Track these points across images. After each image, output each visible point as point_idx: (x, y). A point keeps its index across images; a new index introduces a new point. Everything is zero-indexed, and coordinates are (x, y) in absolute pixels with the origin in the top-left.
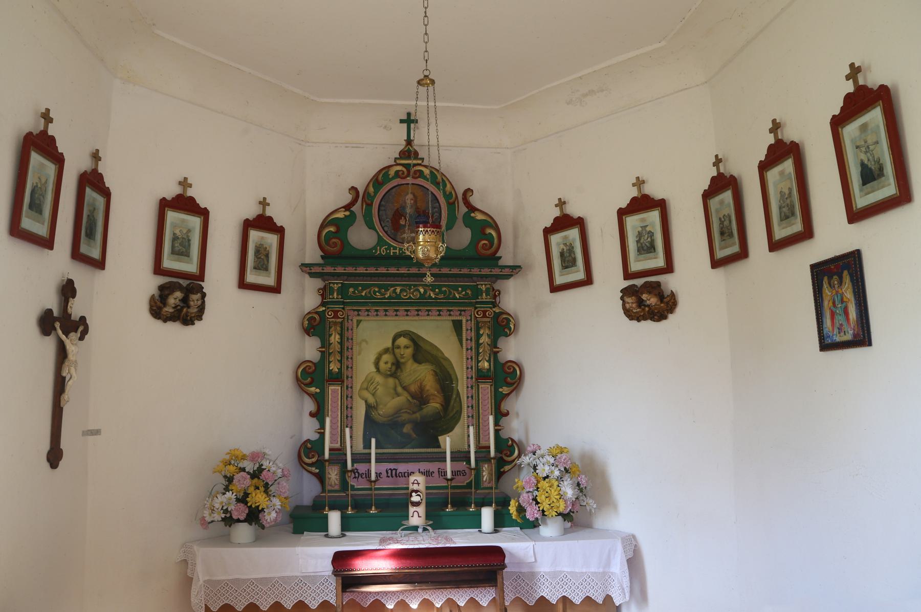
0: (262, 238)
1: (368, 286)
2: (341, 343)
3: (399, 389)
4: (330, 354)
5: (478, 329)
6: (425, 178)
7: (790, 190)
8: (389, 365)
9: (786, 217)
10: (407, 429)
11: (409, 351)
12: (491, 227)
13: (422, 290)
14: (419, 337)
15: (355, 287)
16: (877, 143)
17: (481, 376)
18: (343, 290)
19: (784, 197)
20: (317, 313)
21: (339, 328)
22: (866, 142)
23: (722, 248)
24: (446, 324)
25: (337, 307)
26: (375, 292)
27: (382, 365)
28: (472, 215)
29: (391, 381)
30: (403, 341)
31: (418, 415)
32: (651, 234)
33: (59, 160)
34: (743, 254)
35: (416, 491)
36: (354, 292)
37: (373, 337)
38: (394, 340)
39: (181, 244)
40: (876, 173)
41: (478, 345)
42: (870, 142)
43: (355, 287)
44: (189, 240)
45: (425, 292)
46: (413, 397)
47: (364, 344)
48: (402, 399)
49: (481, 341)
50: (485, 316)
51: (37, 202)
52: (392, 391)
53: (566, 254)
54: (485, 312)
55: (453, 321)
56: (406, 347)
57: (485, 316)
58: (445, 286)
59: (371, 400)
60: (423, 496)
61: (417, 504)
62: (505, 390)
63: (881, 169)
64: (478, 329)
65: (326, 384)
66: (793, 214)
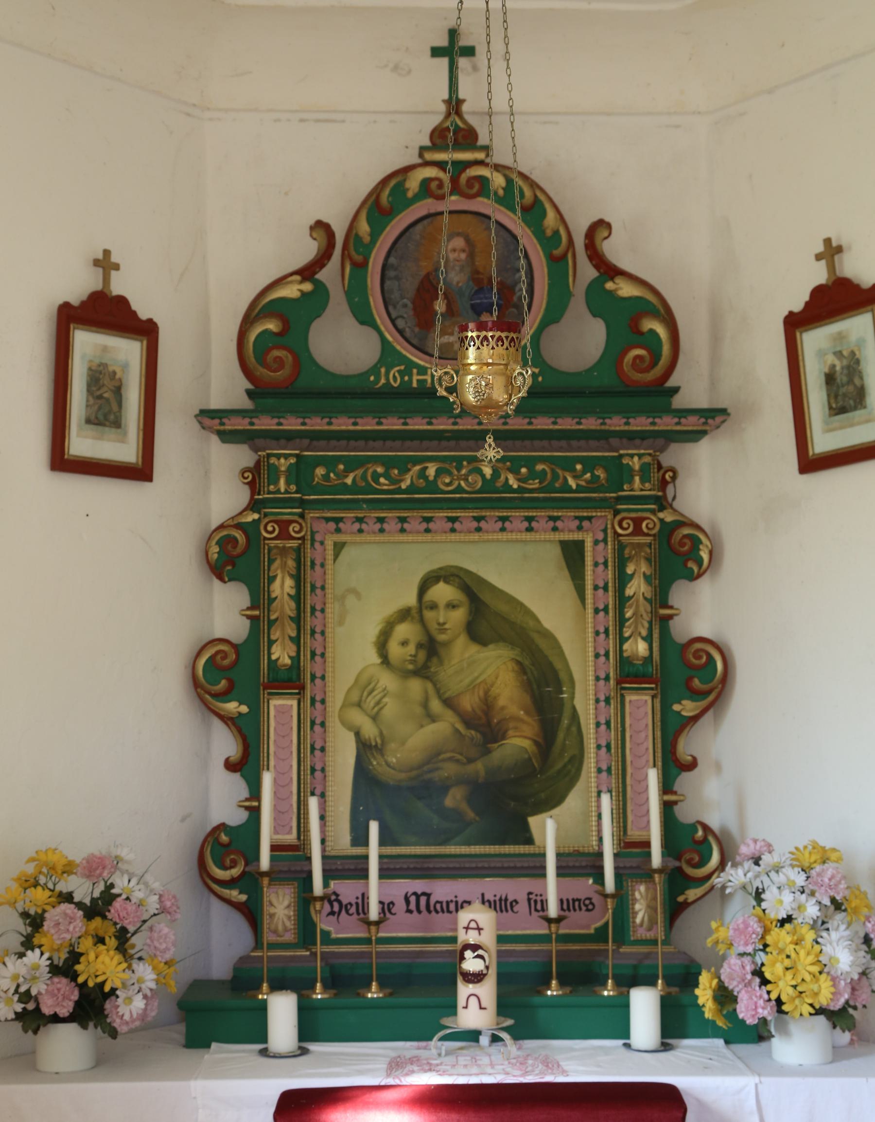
0: (105, 349)
1: (362, 463)
2: (298, 598)
3: (436, 705)
4: (271, 623)
5: (621, 563)
8: (411, 649)
10: (454, 799)
11: (459, 616)
15: (330, 463)
17: (630, 675)
18: (300, 472)
21: (291, 563)
24: (544, 550)
25: (287, 513)
26: (376, 477)
27: (395, 650)
29: (416, 686)
30: (442, 592)
31: (479, 767)
35: (475, 947)
36: (326, 477)
38: (424, 587)
41: (622, 601)
43: (330, 463)
45: (496, 473)
46: (468, 722)
47: (351, 600)
48: (443, 727)
49: (629, 592)
50: (637, 531)
52: (419, 710)
53: (841, 378)
54: (637, 522)
55: (564, 544)
56: (452, 606)
57: (637, 531)
58: (543, 460)
59: (370, 731)
60: (492, 959)
61: (476, 978)
62: (687, 707)
64: (621, 563)
65: (263, 694)
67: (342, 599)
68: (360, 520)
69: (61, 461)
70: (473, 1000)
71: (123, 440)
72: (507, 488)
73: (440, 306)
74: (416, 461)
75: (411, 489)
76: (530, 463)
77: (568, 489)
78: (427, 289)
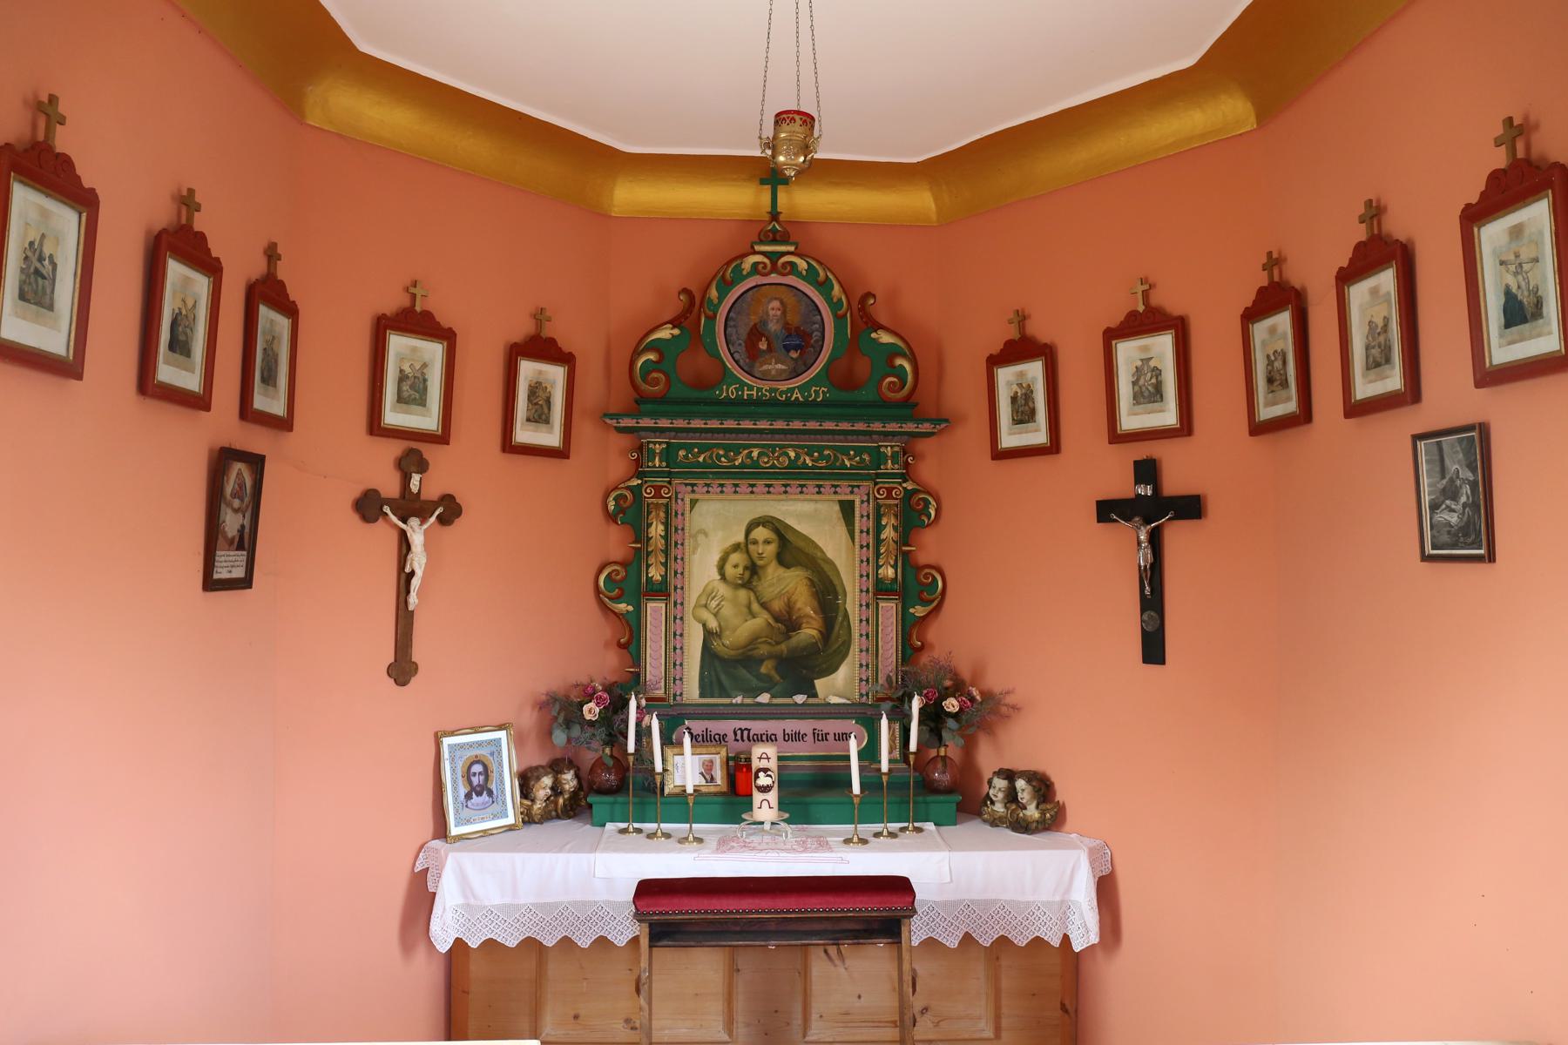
0: (540, 372)
1: (709, 448)
2: (666, 537)
3: (756, 607)
4: (648, 554)
5: (878, 517)
6: (799, 275)
7: (1386, 320)
8: (740, 570)
9: (1377, 363)
10: (766, 668)
11: (771, 550)
12: (904, 356)
13: (792, 454)
14: (788, 527)
15: (689, 448)
16: (1536, 260)
17: (882, 589)
18: (669, 454)
19: (1377, 332)
20: (628, 488)
21: (662, 515)
22: (1517, 256)
23: (1269, 404)
24: (828, 508)
25: (660, 481)
26: (719, 457)
27: (729, 570)
28: (873, 335)
29: (743, 594)
30: (761, 533)
31: (783, 647)
32: (1157, 372)
33: (212, 268)
34: (1305, 415)
35: (765, 770)
36: (686, 457)
37: (714, 527)
38: (749, 530)
39: (412, 387)
40: (1529, 309)
41: (878, 542)
42: (1524, 256)
43: (689, 448)
44: (425, 380)
45: (798, 456)
46: (777, 619)
47: (701, 538)
48: (761, 620)
49: (883, 536)
50: (889, 496)
51: (182, 338)
52: (745, 610)
53: (1021, 401)
54: (889, 491)
55: (841, 502)
56: (767, 542)
57: (889, 496)
58: (827, 447)
59: (713, 624)
60: (775, 775)
61: (765, 789)
62: (919, 611)
63: (1539, 304)
64: (878, 517)
65: (643, 600)
66: (1388, 360)
67: (694, 536)
68: (708, 485)
69: (509, 446)
70: (765, 804)
71: (551, 431)
72: (805, 466)
73: (763, 346)
74: (746, 447)
75: (743, 465)
76: (820, 449)
77: (843, 466)
78: (756, 333)
